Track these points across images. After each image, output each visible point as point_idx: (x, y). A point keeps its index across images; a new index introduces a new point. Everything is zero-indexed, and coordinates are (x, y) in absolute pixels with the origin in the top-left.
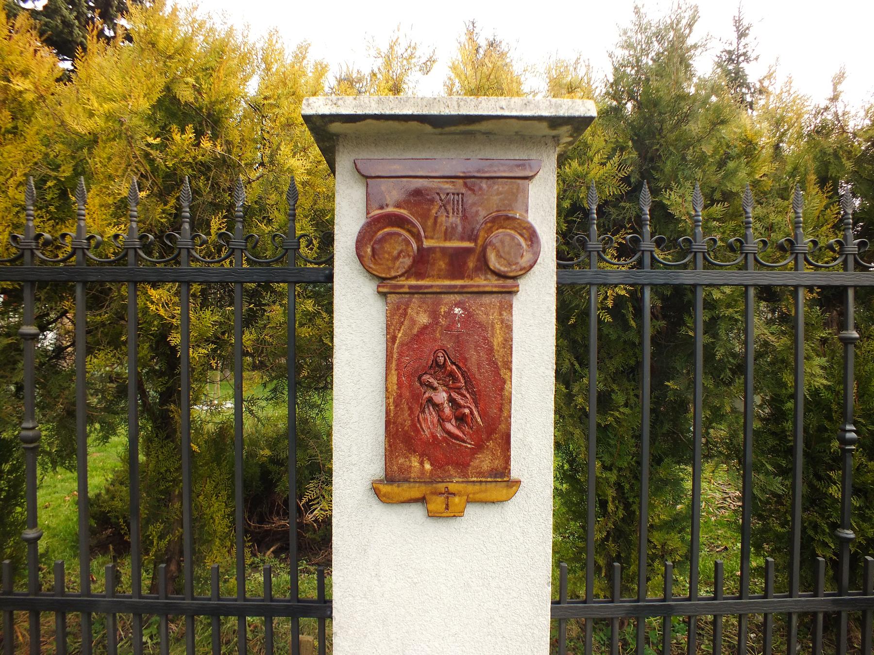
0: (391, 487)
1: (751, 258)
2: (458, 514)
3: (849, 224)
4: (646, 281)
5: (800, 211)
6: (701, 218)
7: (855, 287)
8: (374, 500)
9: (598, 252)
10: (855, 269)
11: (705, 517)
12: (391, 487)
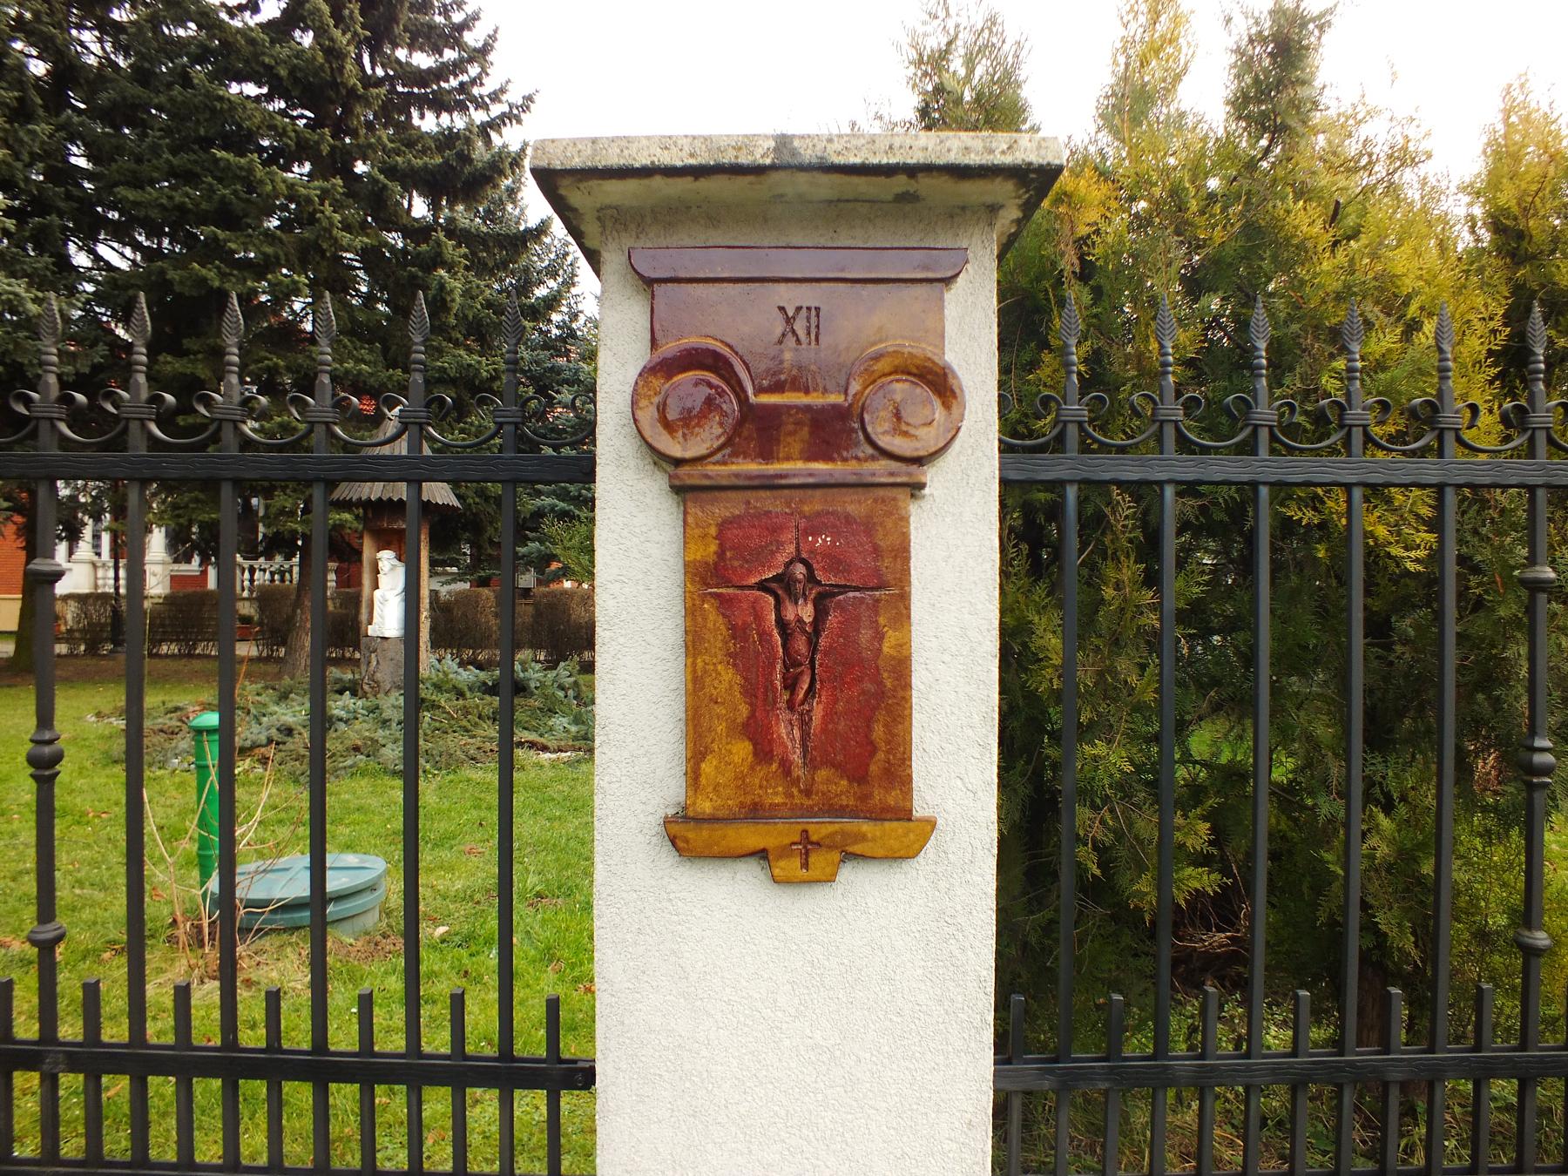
0: (691, 836)
1: (1541, 438)
2: (830, 879)
3: (1539, 372)
4: (1540, 481)
5: (1169, 345)
6: (1171, 359)
7: (1548, 486)
8: (667, 856)
9: (1080, 424)
10: (1273, 451)
11: (192, 887)
12: (691, 836)
